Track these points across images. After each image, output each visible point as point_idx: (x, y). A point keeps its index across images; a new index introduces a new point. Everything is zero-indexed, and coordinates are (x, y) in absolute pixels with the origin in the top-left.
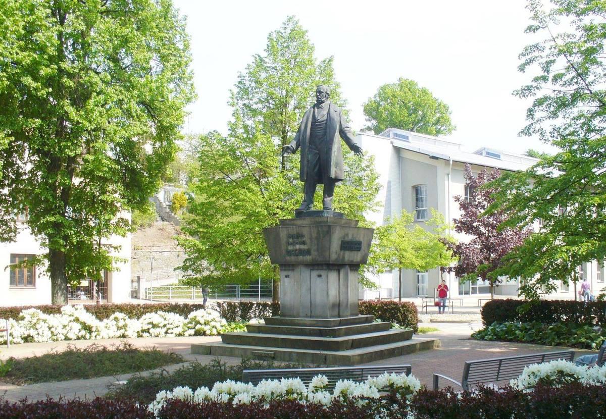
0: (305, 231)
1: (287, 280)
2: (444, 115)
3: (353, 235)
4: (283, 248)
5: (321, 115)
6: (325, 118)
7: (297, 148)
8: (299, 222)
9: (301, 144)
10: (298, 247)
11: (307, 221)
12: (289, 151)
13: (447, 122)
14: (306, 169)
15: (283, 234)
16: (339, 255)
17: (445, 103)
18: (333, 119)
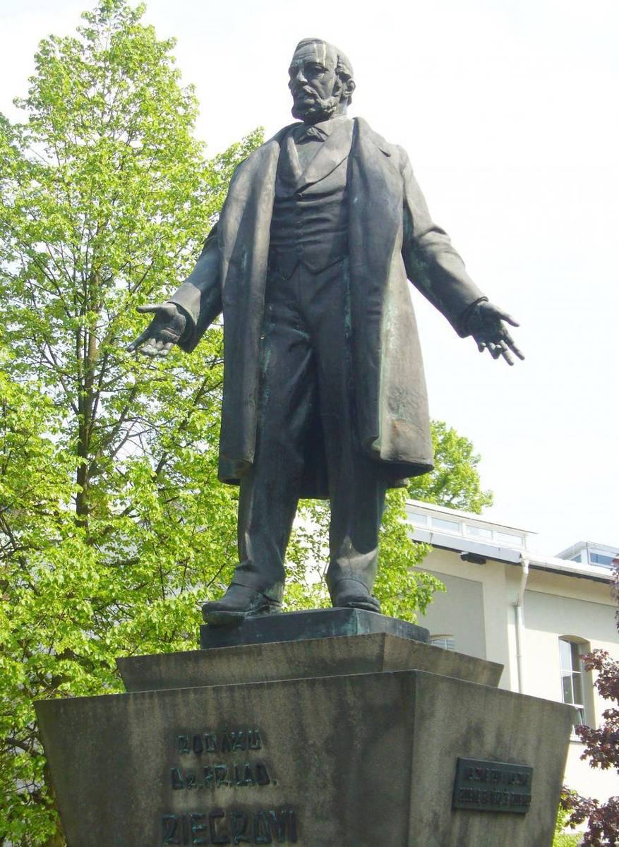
0: (270, 713)
2: (460, 466)
3: (499, 736)
4: (147, 802)
5: (323, 167)
6: (340, 178)
7: (207, 317)
8: (230, 668)
9: (227, 299)
10: (224, 796)
11: (269, 662)
12: (168, 332)
13: (470, 481)
14: (250, 411)
15: (147, 730)
16: (447, 833)
17: (460, 434)
18: (382, 183)
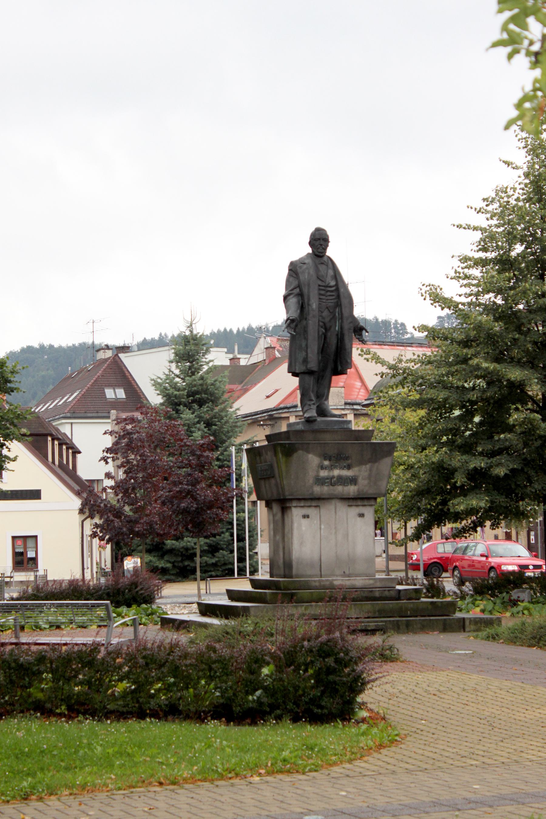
1: (305, 522)
